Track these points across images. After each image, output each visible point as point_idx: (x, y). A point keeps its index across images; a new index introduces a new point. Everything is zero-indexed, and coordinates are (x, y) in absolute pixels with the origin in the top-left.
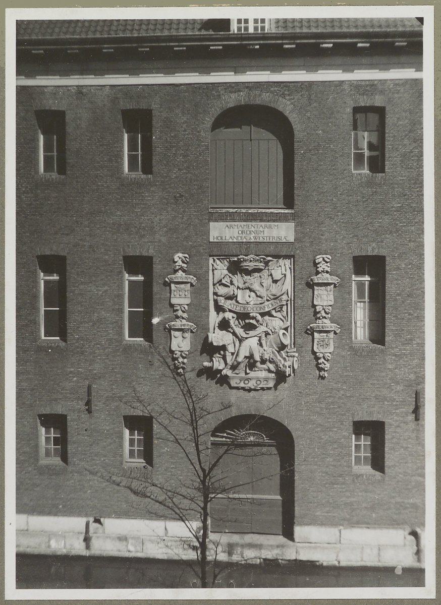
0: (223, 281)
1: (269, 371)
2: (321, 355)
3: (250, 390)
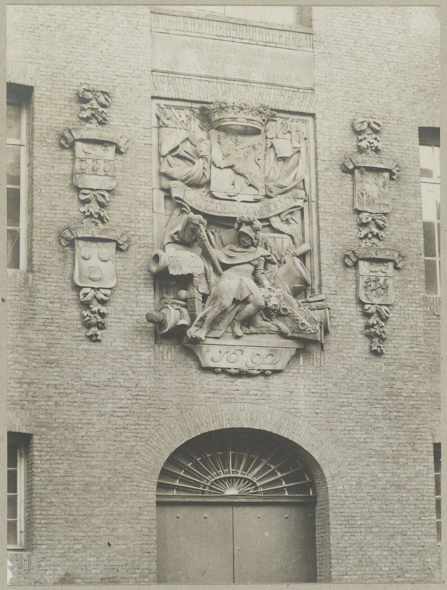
0: (180, 151)
1: (282, 335)
2: (373, 309)
3: (242, 374)
